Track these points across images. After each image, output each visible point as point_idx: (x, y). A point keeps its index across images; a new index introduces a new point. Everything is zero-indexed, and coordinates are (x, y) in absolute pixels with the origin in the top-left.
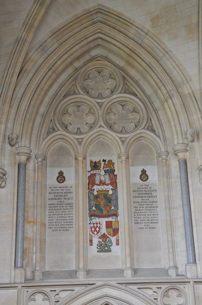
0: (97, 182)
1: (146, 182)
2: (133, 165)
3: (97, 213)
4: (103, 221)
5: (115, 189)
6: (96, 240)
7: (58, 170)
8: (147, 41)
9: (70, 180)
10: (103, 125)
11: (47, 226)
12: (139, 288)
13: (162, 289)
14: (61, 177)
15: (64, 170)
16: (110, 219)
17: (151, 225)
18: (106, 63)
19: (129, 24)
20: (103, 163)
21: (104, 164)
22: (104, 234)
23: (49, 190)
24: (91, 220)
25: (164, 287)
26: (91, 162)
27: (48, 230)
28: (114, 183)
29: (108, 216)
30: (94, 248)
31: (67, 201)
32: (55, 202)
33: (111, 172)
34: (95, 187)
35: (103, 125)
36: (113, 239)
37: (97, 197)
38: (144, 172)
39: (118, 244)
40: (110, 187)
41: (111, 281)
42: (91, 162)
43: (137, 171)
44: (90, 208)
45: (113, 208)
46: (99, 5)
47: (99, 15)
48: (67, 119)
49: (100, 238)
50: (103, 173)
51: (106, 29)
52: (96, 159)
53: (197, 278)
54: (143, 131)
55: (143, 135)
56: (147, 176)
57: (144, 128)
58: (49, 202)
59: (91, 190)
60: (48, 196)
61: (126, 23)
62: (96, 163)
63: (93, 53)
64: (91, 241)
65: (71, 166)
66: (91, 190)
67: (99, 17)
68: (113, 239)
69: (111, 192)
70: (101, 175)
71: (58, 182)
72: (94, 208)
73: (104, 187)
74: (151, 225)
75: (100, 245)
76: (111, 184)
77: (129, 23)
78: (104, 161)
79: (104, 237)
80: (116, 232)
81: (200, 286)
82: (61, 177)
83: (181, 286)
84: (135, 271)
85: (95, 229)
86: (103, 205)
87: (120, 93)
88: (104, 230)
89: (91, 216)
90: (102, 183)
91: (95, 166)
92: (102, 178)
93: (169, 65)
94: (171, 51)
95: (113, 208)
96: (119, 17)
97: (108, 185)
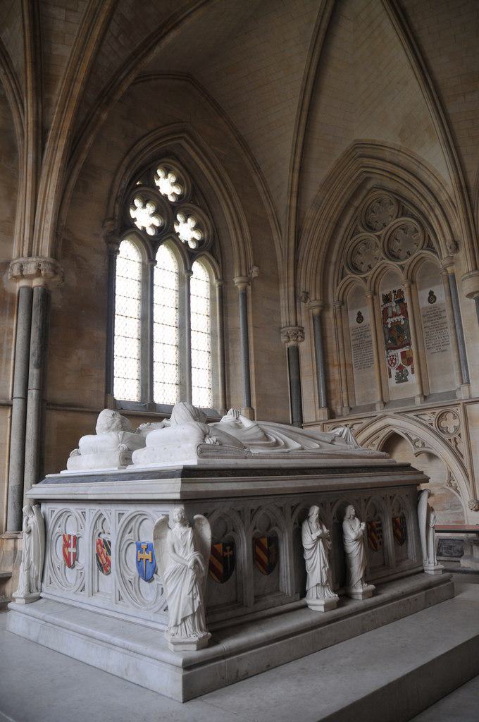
0: (390, 315)
1: (435, 304)
2: (421, 289)
3: (393, 345)
4: (399, 352)
5: (406, 318)
6: (394, 372)
7: (428, 291)
8: (402, 159)
9: (368, 318)
10: (384, 257)
11: (354, 366)
12: (417, 416)
13: (437, 414)
14: (360, 318)
15: (432, 289)
16: (404, 349)
17: (443, 348)
18: (380, 192)
19: (383, 148)
20: (393, 295)
21: (395, 295)
22: (400, 365)
23: (351, 332)
24: (388, 353)
25: (438, 411)
26: (383, 295)
27: (354, 369)
28: (405, 313)
29: (402, 347)
30: (393, 381)
31: (366, 340)
32: (357, 342)
33: (401, 301)
34: (389, 321)
35: (384, 257)
36: (409, 368)
37: (390, 330)
38: (431, 293)
39: (413, 372)
40: (402, 317)
41: (389, 411)
42: (383, 295)
43: (424, 294)
44: (386, 342)
45: (406, 337)
46: (355, 140)
47: (357, 150)
48: (359, 259)
49: (397, 369)
50: (394, 304)
51: (366, 161)
52: (386, 292)
53: (470, 398)
54: (420, 251)
55: (423, 255)
56: (435, 297)
57: (422, 248)
58: (353, 343)
59: (385, 324)
60: (352, 338)
61: (380, 147)
62: (387, 296)
63: (369, 186)
64: (390, 373)
65: (366, 305)
66: (385, 324)
67: (359, 152)
68: (409, 368)
69: (403, 322)
70: (394, 307)
71: (358, 322)
72: (389, 341)
73: (395, 319)
74: (443, 348)
75: (398, 376)
76: (402, 314)
77: (382, 146)
78: (394, 292)
79: (400, 368)
80: (409, 361)
81: (476, 406)
82: (360, 318)
83: (454, 409)
84: (425, 398)
85: (392, 361)
86: (396, 337)
87: (397, 217)
88: (400, 362)
89: (388, 349)
90: (395, 315)
91: (387, 299)
92: (394, 310)
93: (425, 176)
94: (424, 160)
95: (406, 337)
96: (373, 145)
97: (400, 315)
